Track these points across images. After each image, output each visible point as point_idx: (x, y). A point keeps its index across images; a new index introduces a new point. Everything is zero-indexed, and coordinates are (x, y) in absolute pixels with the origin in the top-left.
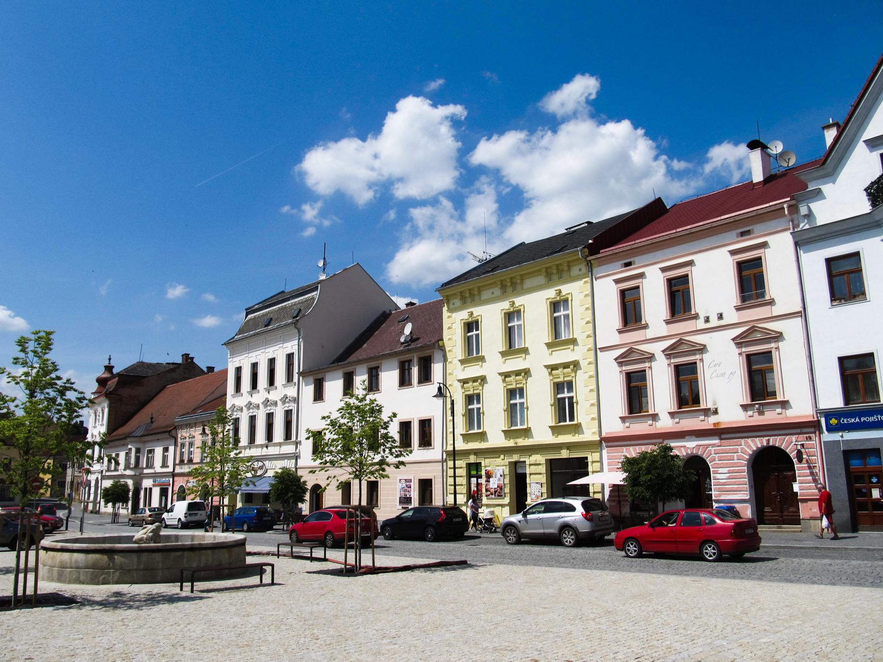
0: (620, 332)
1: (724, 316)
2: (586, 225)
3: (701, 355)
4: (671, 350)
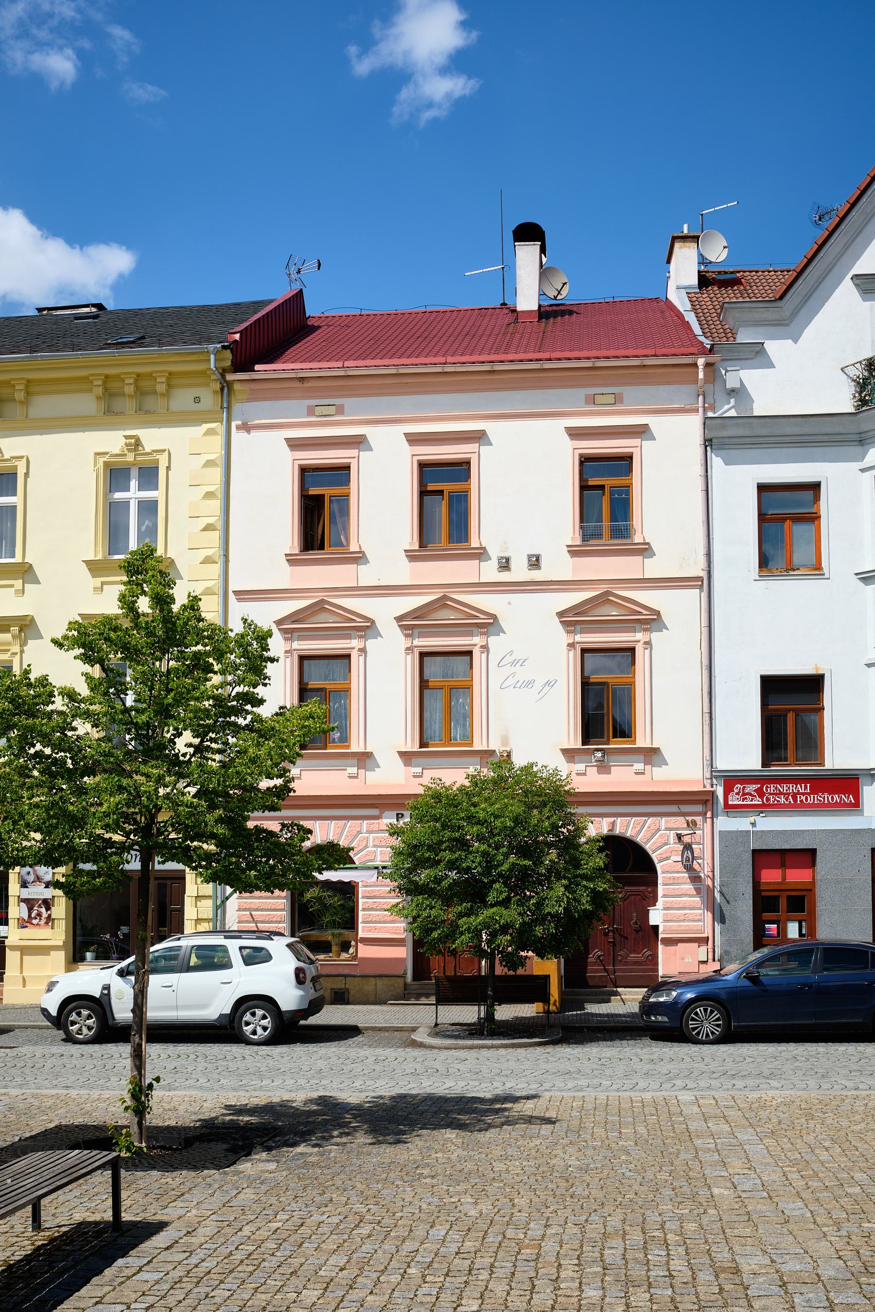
0: (412, 556)
1: (543, 562)
2: (94, 310)
3: (484, 638)
4: (294, 622)
